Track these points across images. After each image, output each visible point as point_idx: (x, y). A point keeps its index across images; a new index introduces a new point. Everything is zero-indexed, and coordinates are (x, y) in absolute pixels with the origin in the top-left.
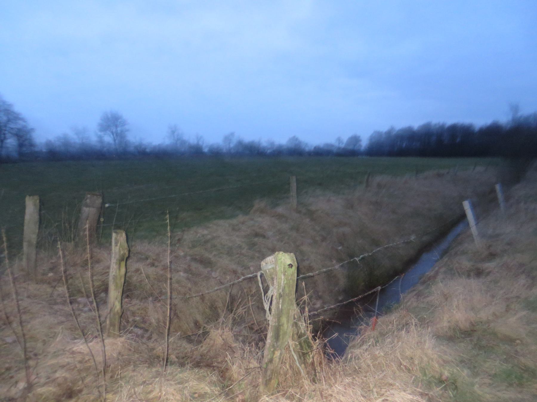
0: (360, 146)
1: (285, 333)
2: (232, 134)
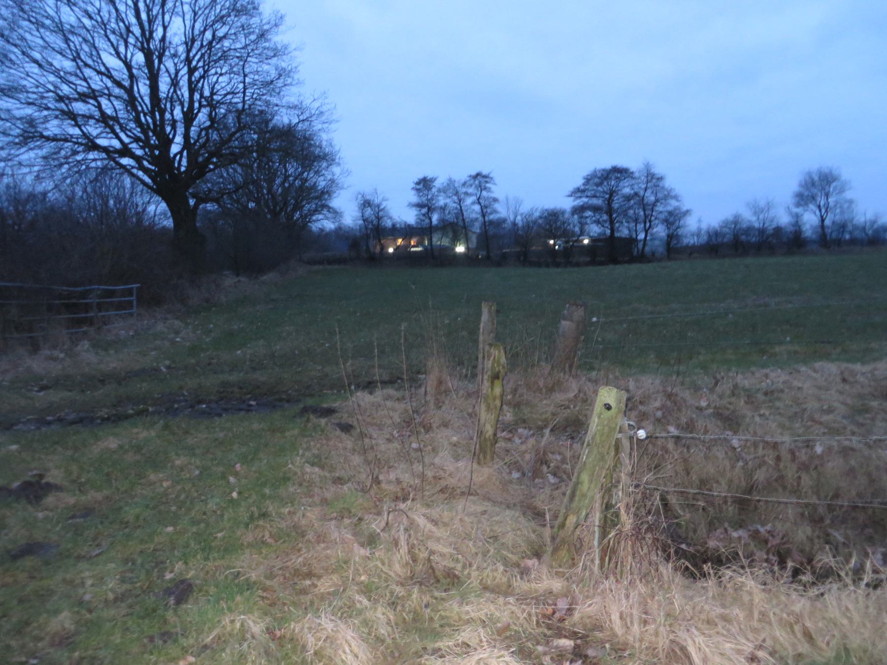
1: (584, 496)
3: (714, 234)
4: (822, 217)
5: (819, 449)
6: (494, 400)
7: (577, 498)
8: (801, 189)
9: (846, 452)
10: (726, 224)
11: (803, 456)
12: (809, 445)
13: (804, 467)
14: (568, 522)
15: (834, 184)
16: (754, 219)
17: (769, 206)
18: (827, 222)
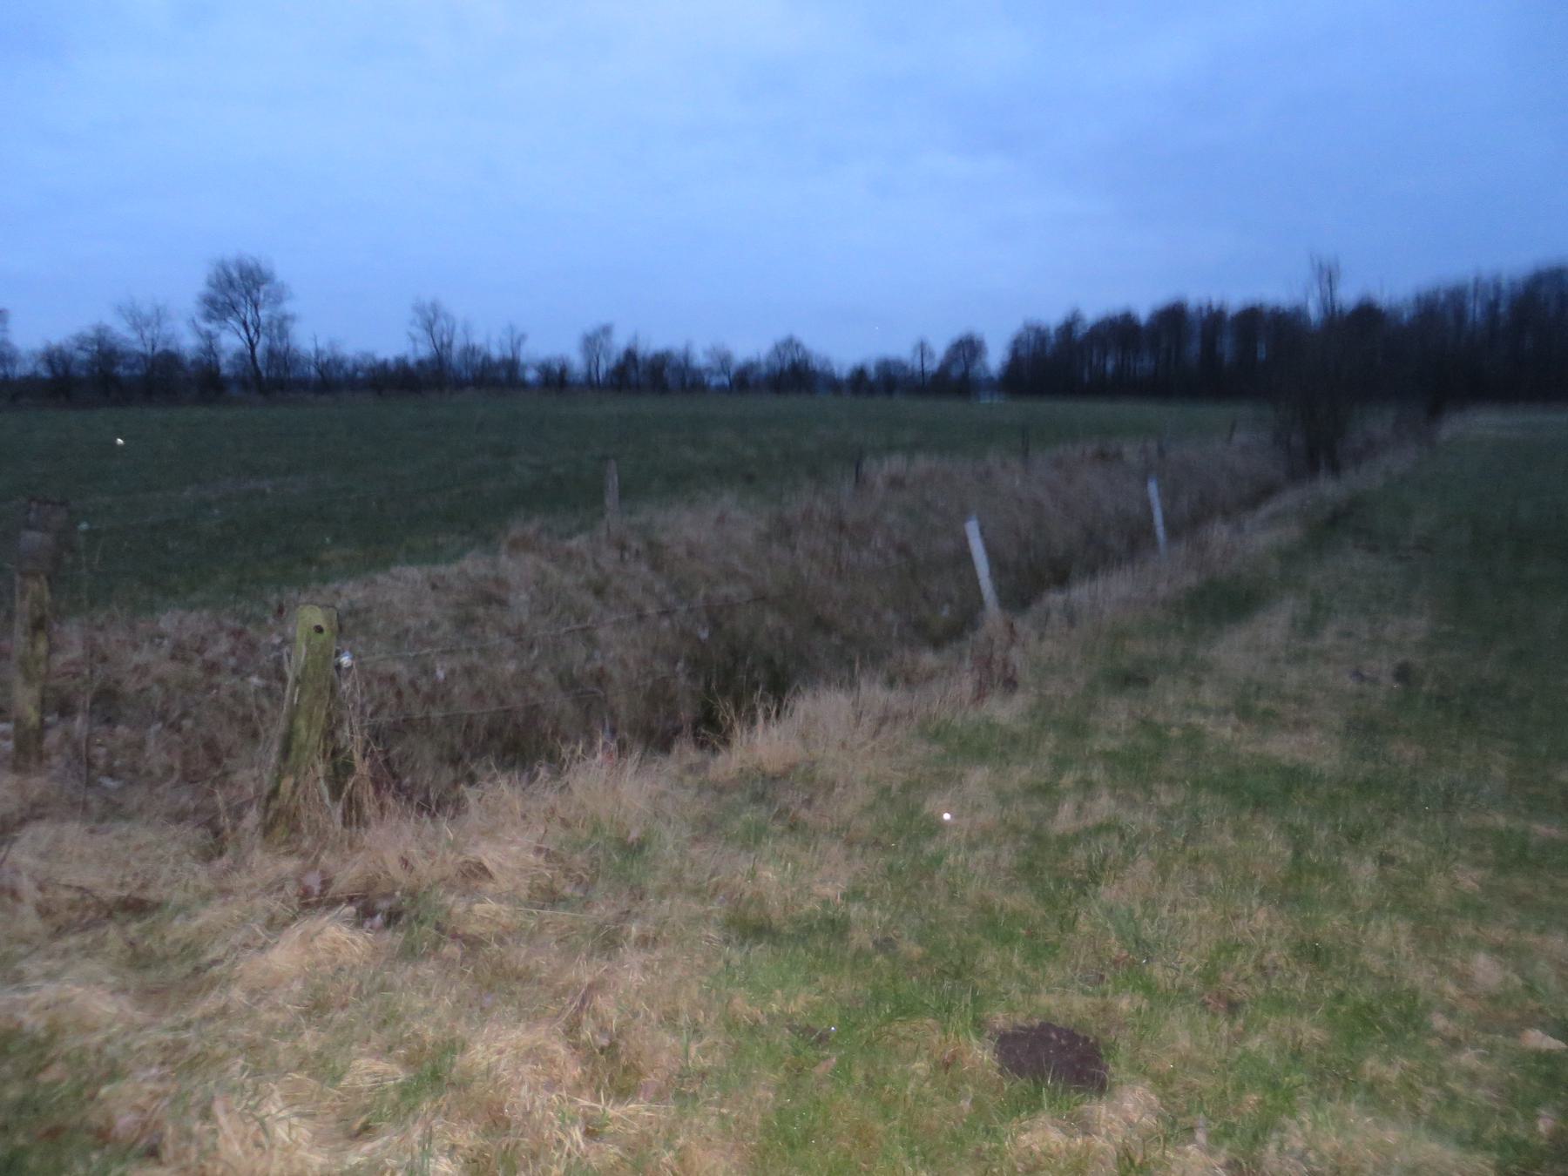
0: (985, 368)
1: (302, 748)
2: (606, 330)
3: (55, 358)
4: (250, 341)
5: (441, 674)
6: (37, 663)
7: (293, 754)
8: (212, 291)
9: (470, 672)
10: (82, 343)
11: (424, 685)
12: (428, 671)
13: (430, 699)
14: (282, 789)
15: (264, 288)
16: (133, 336)
17: (159, 315)
18: (259, 350)
